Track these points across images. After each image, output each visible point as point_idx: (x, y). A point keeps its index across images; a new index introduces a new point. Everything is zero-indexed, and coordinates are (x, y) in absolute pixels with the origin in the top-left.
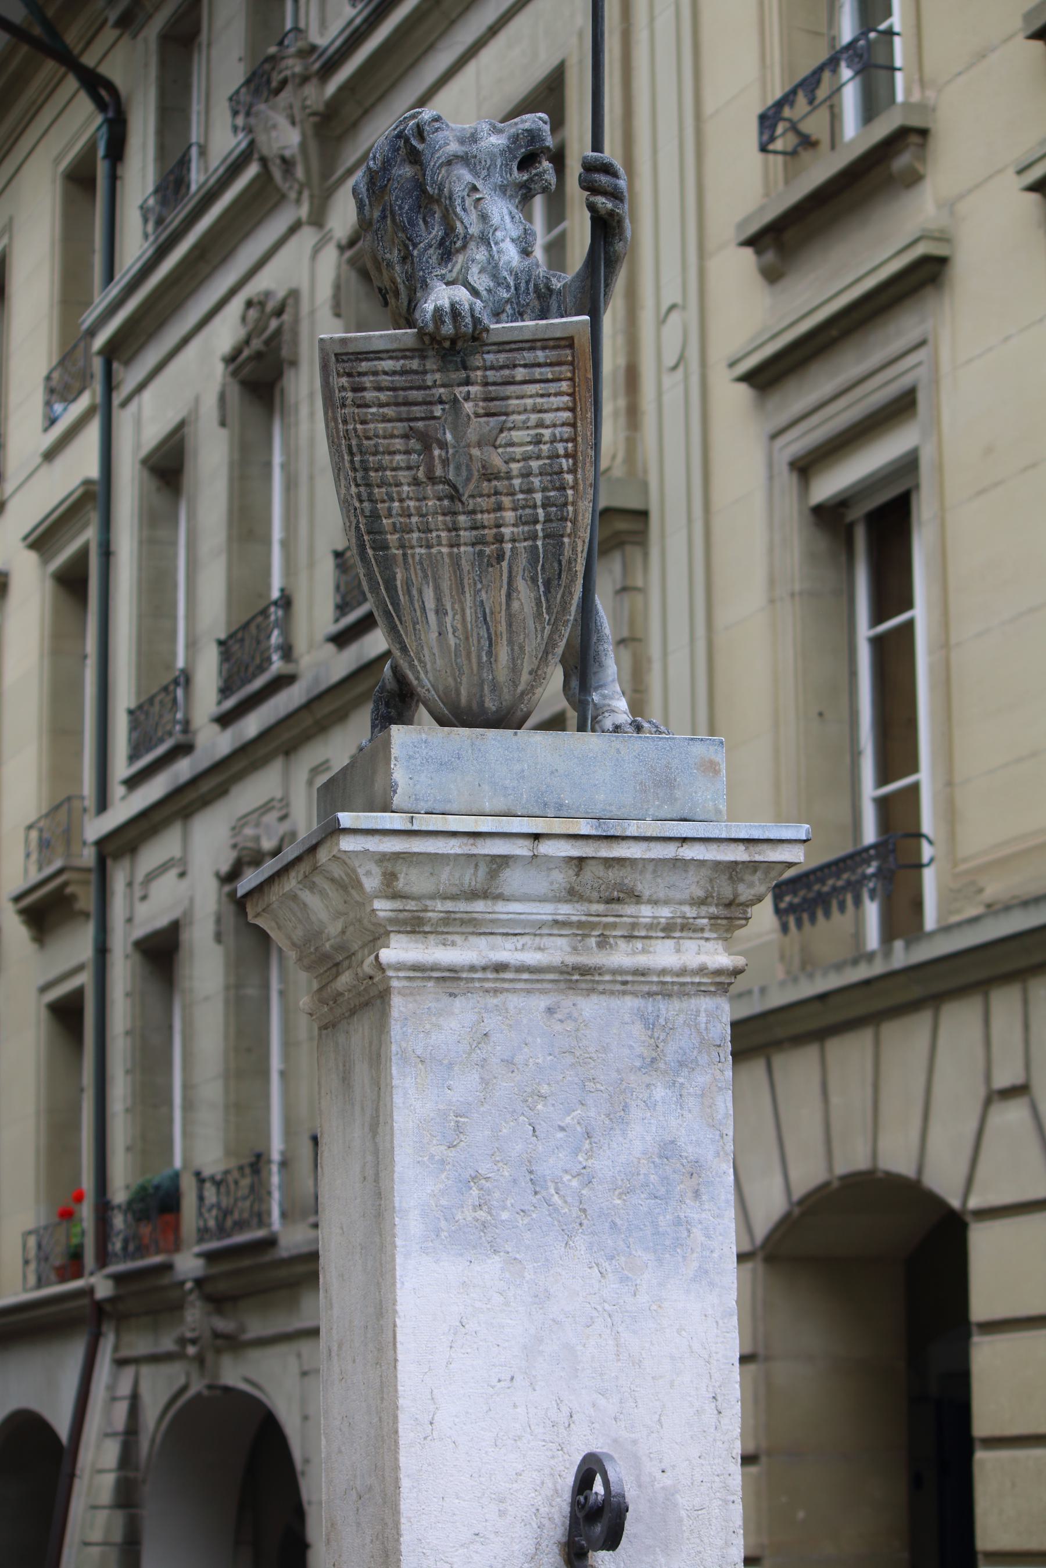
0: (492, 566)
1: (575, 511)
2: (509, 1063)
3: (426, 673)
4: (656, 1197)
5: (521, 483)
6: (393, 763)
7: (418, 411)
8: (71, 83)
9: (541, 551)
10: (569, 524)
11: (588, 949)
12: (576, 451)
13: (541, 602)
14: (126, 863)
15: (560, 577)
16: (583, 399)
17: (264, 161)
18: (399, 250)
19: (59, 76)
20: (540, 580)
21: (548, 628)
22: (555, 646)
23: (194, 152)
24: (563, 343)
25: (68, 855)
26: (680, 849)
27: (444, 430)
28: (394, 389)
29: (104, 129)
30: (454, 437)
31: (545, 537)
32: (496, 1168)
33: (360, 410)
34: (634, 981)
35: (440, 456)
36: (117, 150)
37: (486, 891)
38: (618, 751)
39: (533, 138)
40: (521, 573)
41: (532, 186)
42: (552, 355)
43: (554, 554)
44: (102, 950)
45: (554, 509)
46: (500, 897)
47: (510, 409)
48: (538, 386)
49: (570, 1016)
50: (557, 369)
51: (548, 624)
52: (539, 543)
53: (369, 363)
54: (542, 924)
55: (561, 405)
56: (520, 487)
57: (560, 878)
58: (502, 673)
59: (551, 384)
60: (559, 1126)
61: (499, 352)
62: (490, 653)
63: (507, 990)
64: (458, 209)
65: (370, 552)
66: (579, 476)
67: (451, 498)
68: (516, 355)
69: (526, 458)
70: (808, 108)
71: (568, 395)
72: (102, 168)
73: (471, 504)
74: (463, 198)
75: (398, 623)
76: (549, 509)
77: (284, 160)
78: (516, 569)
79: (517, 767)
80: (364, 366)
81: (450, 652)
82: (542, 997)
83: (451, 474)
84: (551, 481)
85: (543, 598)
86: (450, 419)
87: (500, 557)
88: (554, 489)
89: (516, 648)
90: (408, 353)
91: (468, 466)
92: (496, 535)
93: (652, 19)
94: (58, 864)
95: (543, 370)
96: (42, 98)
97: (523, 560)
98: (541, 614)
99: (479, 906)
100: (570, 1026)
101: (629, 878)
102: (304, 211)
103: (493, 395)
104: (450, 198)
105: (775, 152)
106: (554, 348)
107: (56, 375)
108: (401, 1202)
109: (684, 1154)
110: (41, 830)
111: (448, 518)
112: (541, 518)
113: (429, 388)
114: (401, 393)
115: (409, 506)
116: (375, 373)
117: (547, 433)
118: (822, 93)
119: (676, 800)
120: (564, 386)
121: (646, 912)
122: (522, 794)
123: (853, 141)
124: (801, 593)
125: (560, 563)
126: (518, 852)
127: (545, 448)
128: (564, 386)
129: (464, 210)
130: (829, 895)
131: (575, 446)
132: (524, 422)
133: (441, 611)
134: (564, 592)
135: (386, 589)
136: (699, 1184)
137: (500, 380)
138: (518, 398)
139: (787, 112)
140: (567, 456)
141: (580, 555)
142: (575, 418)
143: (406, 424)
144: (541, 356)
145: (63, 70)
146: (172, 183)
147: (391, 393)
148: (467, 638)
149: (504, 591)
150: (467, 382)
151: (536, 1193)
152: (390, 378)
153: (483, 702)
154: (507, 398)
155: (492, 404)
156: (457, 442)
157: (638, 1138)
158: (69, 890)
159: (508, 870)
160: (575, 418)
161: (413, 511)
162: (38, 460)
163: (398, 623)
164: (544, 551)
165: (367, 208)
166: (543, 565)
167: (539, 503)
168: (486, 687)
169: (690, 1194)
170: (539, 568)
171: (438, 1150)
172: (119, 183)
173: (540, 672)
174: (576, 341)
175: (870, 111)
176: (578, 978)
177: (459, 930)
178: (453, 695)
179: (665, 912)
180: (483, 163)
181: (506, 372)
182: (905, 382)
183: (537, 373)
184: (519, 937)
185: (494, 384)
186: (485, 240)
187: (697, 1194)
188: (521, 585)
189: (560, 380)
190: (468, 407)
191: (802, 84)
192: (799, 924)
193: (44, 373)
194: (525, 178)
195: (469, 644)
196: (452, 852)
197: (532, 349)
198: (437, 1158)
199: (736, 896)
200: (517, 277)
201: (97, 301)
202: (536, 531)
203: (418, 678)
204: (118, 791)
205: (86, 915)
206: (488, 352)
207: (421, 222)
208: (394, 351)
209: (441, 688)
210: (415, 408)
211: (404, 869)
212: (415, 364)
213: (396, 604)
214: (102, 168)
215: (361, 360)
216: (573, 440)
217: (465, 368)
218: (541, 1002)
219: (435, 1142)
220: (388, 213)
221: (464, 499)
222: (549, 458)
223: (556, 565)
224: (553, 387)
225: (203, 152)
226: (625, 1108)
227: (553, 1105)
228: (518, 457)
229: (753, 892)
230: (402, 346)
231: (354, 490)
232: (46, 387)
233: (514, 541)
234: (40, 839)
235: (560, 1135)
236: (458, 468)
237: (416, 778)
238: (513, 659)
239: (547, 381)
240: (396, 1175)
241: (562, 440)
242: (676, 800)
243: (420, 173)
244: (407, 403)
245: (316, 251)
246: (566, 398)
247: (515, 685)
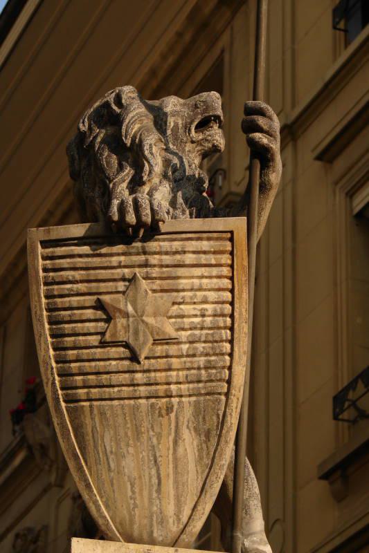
0: (162, 417)
5: (188, 349)
17: (30, 448)
18: (99, 187)
24: (224, 235)
40: (186, 423)
45: (214, 371)
47: (181, 287)
56: (187, 352)
59: (214, 268)
64: (146, 153)
65: (63, 404)
68: (187, 243)
73: (146, 364)
74: (151, 145)
75: (83, 464)
76: (210, 371)
77: (42, 446)
78: (181, 418)
84: (212, 348)
87: (169, 409)
90: (99, 240)
92: (166, 390)
93: (268, 345)
95: (207, 256)
102: (53, 478)
105: (343, 420)
117: (209, 308)
127: (208, 319)
129: (152, 154)
132: (191, 298)
139: (351, 395)
141: (234, 410)
142: (233, 298)
144: (205, 245)
149: (171, 438)
150: (146, 265)
153: (152, 532)
154: (178, 278)
160: (233, 298)
163: (83, 464)
165: (76, 162)
181: (178, 257)
183: (203, 259)
185: (167, 266)
194: (200, 137)
224: (215, 271)
245: (59, 502)
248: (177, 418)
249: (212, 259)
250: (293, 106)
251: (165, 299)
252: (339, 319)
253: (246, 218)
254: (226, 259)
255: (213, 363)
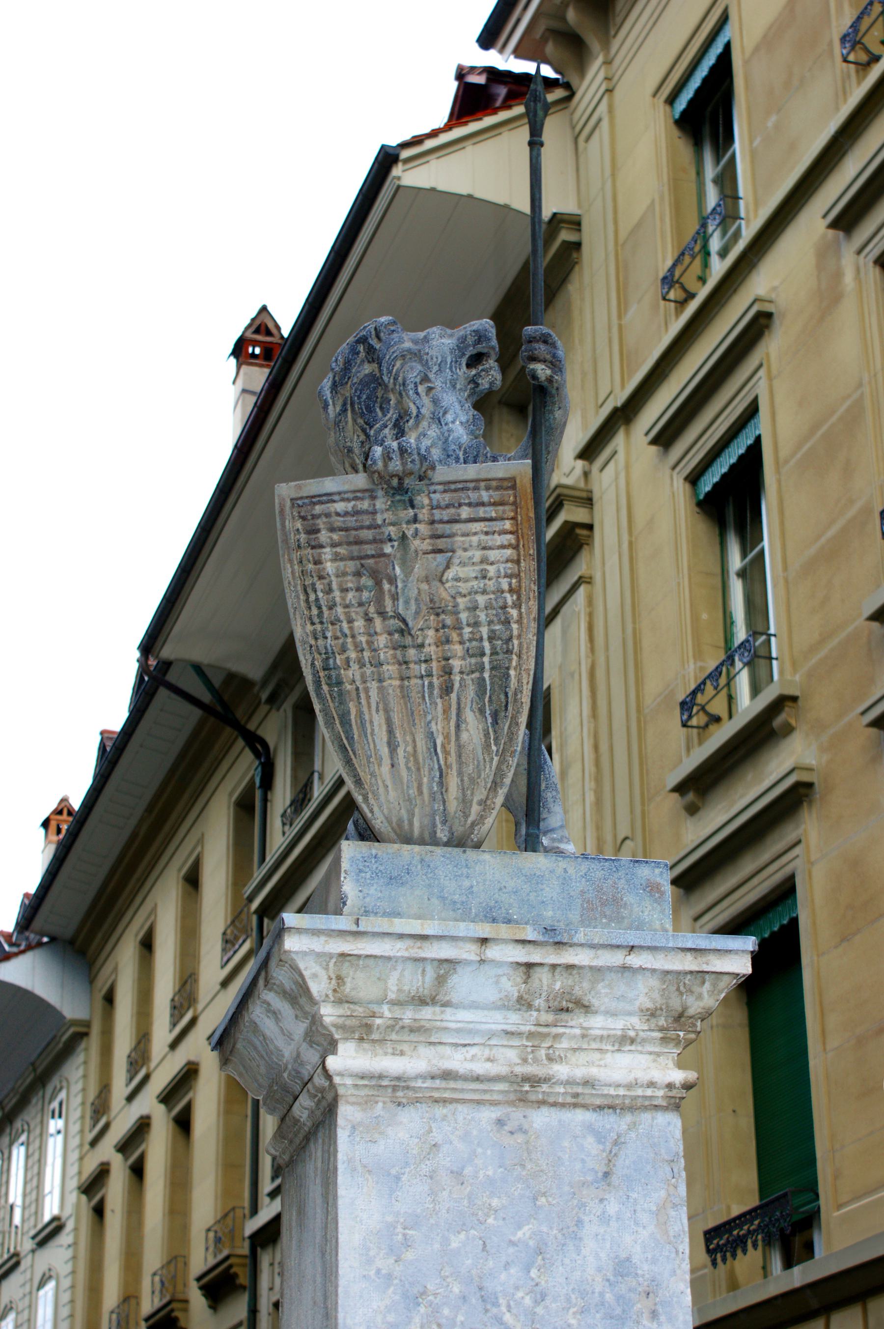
1: (520, 645)
2: (457, 1174)
3: (380, 807)
4: (611, 1318)
5: (468, 617)
6: (343, 875)
7: (369, 549)
8: (241, 743)
9: (488, 682)
10: (514, 657)
11: (536, 1060)
12: (520, 586)
13: (489, 733)
14: (270, 1250)
15: (506, 709)
16: (526, 537)
19: (234, 737)
20: (488, 712)
21: (496, 759)
22: (503, 776)
23: (316, 776)
25: (233, 1247)
26: (628, 958)
27: (393, 565)
28: (347, 530)
29: (259, 769)
30: (402, 570)
31: (492, 669)
32: (445, 1284)
33: (314, 551)
34: (582, 1097)
35: (390, 591)
36: (267, 782)
37: (434, 998)
38: (565, 870)
39: (480, 337)
40: (469, 705)
41: (480, 381)
42: (496, 495)
43: (500, 686)
44: (253, 1311)
45: (500, 642)
46: (446, 1004)
48: (482, 524)
49: (521, 1130)
50: (501, 508)
51: (496, 755)
52: (486, 675)
53: (323, 506)
54: (492, 1035)
55: (506, 543)
57: (511, 986)
58: (453, 806)
59: (494, 523)
60: (510, 1241)
61: (445, 491)
62: (441, 784)
63: (457, 1101)
66: (523, 610)
67: (401, 632)
69: (473, 592)
70: (714, 692)
71: (511, 533)
72: (258, 794)
76: (495, 642)
78: (463, 700)
79: (467, 883)
80: (318, 509)
81: (402, 783)
82: (492, 1108)
83: (401, 608)
85: (491, 730)
86: (398, 555)
88: (500, 622)
89: (466, 779)
90: (359, 494)
91: (416, 600)
94: (225, 1252)
95: (487, 509)
96: (221, 756)
97: (471, 692)
98: (489, 746)
99: (427, 1013)
100: (520, 1138)
101: (582, 988)
103: (439, 532)
104: (404, 384)
105: (692, 727)
106: (497, 488)
107: (229, 931)
108: (345, 1318)
109: (640, 1272)
110: (216, 1232)
111: (398, 652)
112: (488, 651)
113: (379, 527)
114: (353, 532)
115: (361, 641)
116: (328, 515)
118: (723, 681)
119: (623, 918)
120: (508, 525)
121: (597, 1023)
122: (471, 909)
123: (747, 709)
124: (717, 1026)
125: (506, 694)
126: (465, 956)
128: (508, 525)
129: (417, 394)
130: (745, 1236)
131: (519, 582)
133: (392, 746)
134: (510, 724)
135: (341, 723)
136: (655, 1304)
137: (446, 518)
138: (463, 535)
140: (511, 591)
141: (525, 687)
142: (519, 555)
143: (358, 562)
145: (236, 733)
146: (301, 799)
147: (343, 533)
148: (418, 769)
150: (415, 520)
151: (487, 1311)
152: (342, 519)
153: (435, 833)
155: (439, 541)
156: (406, 576)
157: (592, 1256)
158: (233, 1270)
159: (455, 976)
160: (519, 555)
161: (365, 645)
162: (218, 987)
164: (492, 683)
166: (490, 697)
167: (485, 636)
168: (437, 818)
169: (646, 1315)
170: (487, 700)
171: (384, 1263)
172: (269, 804)
173: (489, 802)
174: (518, 482)
175: (755, 690)
176: (527, 1090)
177: (406, 1038)
178: (406, 827)
179: (617, 1025)
180: (435, 359)
181: (452, 511)
182: (787, 871)
183: (481, 512)
184: (468, 1048)
185: (441, 522)
186: (438, 420)
187: (654, 1315)
188: (470, 716)
189: (503, 519)
190: (416, 544)
191: (710, 676)
192: (724, 1260)
193: (222, 930)
195: (420, 775)
196: (399, 954)
197: (476, 488)
198: (384, 1272)
199: (685, 1009)
200: (465, 452)
201: (255, 875)
202: (483, 663)
203: (372, 811)
204: (264, 1200)
205: (244, 1288)
206: (435, 492)
207: (378, 410)
208: (345, 492)
209: (394, 820)
210: (366, 546)
211: (351, 973)
212: (365, 505)
213: (350, 738)
214: (258, 794)
215: (315, 504)
216: (518, 576)
217: (413, 506)
218: (488, 1115)
219: (381, 1255)
220: (349, 406)
221: (413, 632)
222: (493, 593)
223: (502, 697)
224: (498, 526)
225: (321, 777)
226: (579, 1223)
227: (504, 1219)
228: (464, 591)
229: (702, 1004)
230: (352, 488)
231: (309, 628)
232: (223, 939)
233: (461, 673)
234: (215, 1237)
235: (511, 1250)
236: (407, 602)
237: (366, 891)
238: (463, 789)
239: (491, 519)
240: (340, 1290)
241: (506, 576)
242: (623, 918)
243: (377, 370)
244: (358, 542)
246: (509, 536)
247: (466, 816)
248: (459, 699)
249: (492, 512)
250: (623, 386)
251: (438, 560)
252: (683, 623)
253: (530, 461)
254: (509, 511)
255: (497, 633)
